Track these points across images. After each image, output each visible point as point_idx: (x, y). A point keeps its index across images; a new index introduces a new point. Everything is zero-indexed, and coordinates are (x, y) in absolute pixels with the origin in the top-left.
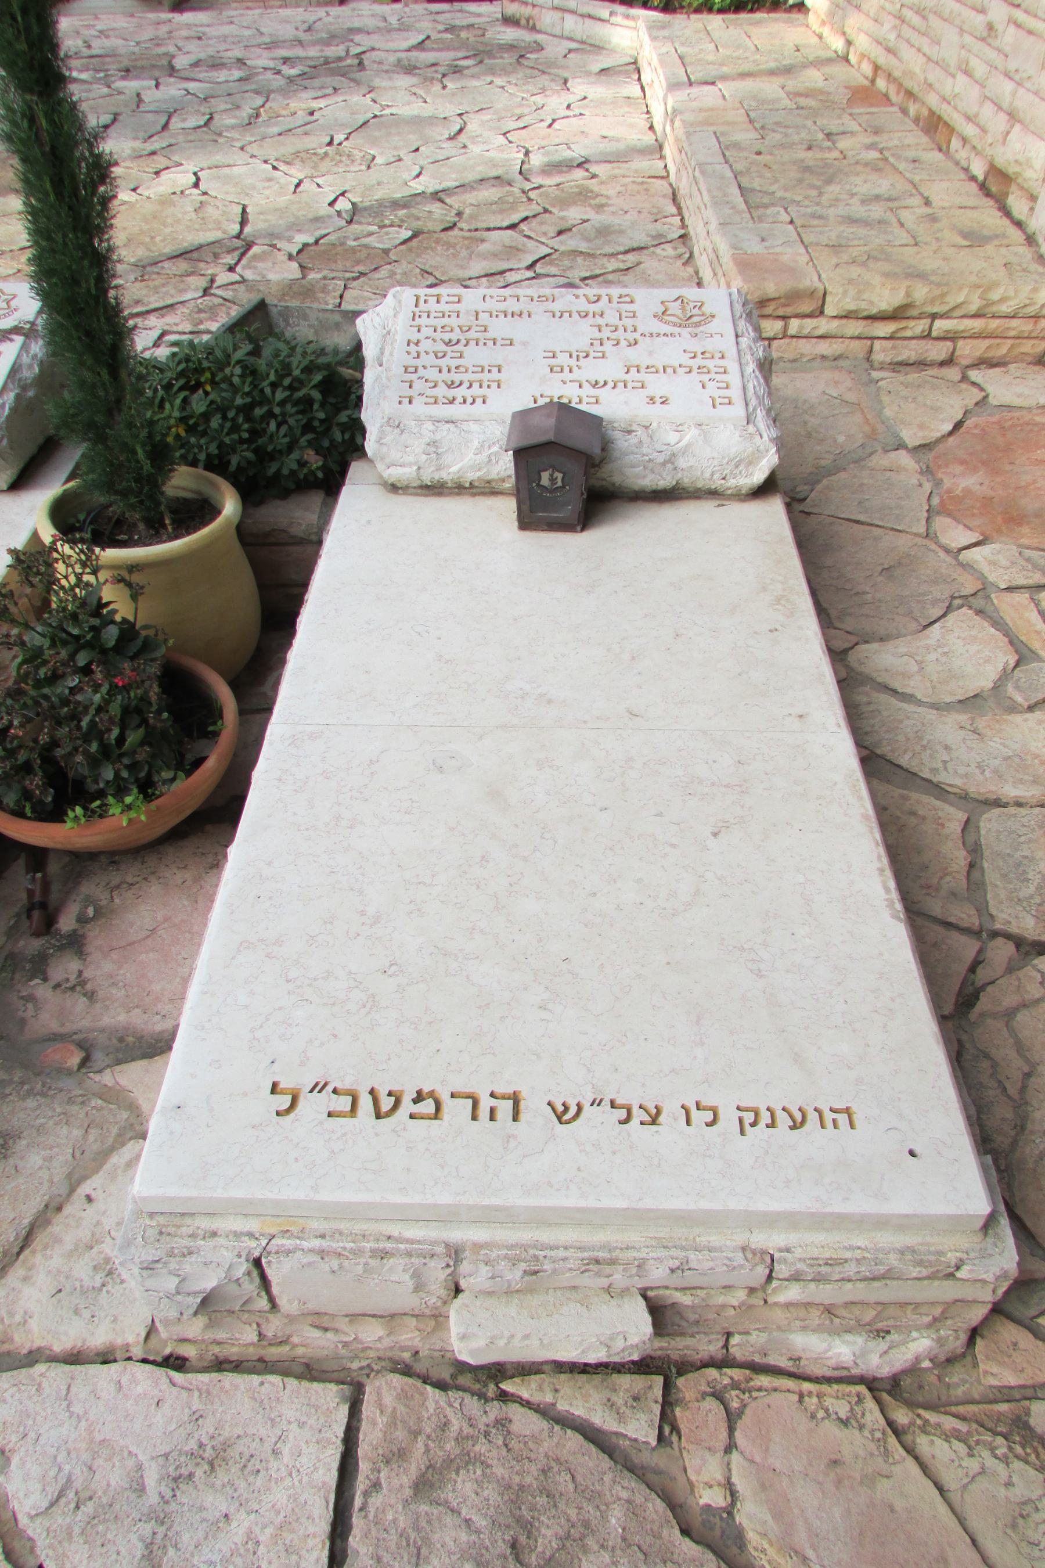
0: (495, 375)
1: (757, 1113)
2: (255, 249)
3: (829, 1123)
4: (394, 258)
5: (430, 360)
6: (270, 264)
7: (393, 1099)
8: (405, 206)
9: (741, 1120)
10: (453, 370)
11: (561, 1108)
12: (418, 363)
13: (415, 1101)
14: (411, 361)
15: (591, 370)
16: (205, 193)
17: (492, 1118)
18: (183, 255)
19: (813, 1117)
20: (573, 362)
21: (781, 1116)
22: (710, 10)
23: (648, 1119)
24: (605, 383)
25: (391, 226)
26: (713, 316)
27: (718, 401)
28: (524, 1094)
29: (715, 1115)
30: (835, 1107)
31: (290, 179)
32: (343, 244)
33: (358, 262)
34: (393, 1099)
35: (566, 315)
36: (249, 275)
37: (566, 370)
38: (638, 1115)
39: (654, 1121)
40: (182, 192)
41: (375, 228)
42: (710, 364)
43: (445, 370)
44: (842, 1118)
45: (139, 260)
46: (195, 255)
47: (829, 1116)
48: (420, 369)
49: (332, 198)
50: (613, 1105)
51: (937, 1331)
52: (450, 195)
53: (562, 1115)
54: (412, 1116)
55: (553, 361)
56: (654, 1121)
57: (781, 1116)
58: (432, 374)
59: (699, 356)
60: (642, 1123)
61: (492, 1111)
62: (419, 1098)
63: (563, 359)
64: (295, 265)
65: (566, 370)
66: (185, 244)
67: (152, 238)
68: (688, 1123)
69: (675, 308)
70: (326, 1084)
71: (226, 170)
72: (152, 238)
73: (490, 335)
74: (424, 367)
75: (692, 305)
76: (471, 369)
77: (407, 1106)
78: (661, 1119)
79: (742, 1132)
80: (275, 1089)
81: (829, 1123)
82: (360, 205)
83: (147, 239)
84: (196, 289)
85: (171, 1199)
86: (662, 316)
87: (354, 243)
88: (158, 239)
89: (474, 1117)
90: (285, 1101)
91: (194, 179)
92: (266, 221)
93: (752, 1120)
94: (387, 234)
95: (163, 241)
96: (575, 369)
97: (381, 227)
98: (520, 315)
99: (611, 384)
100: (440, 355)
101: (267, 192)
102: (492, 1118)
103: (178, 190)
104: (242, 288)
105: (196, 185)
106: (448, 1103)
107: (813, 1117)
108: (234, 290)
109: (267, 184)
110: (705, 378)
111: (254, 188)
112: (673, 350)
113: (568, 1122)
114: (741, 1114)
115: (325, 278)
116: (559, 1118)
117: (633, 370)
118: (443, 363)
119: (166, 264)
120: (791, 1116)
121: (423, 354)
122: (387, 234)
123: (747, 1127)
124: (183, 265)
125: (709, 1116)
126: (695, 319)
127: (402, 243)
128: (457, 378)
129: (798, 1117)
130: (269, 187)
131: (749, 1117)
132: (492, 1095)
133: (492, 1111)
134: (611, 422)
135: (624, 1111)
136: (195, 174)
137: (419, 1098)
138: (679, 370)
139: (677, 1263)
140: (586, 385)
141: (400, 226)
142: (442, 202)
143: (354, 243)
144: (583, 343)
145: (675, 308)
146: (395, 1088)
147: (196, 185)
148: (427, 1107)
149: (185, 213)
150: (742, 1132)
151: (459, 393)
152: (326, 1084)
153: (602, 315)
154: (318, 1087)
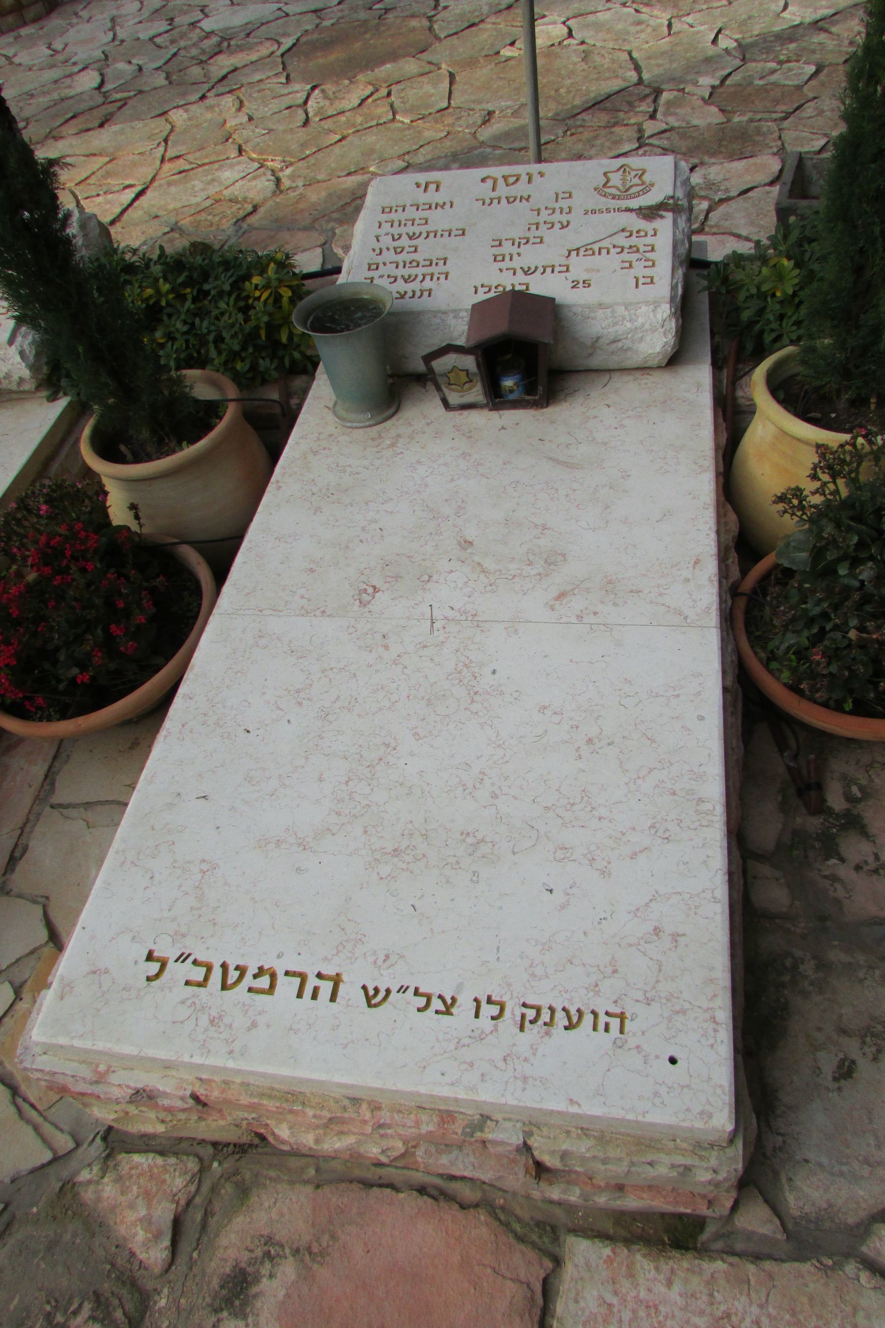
0: (441, 268)
1: (538, 1010)
2: (665, 96)
3: (601, 1026)
4: (811, 95)
5: (389, 256)
6: (689, 110)
7: (238, 973)
8: (791, 40)
9: (523, 1016)
10: (408, 265)
11: (371, 992)
12: (380, 260)
13: (255, 976)
15: (530, 256)
16: (583, 43)
17: (314, 996)
18: (597, 105)
19: (588, 1019)
20: (514, 250)
21: (560, 1015)
23: (443, 1008)
25: (788, 61)
26: (652, 185)
28: (345, 977)
29: (502, 1010)
30: (610, 1011)
31: (659, 21)
32: (751, 83)
33: (777, 102)
34: (238, 973)
36: (673, 121)
37: (507, 258)
38: (437, 1004)
39: (448, 1012)
40: (560, 43)
41: (773, 65)
42: (640, 242)
43: (401, 265)
44: (615, 1023)
45: (557, 114)
46: (608, 104)
47: (603, 1019)
48: (381, 266)
49: (712, 36)
50: (417, 992)
52: (834, 24)
53: (373, 998)
54: (250, 990)
55: (497, 251)
56: (448, 1012)
57: (560, 1015)
58: (391, 269)
60: (437, 1012)
61: (316, 990)
62: (261, 972)
63: (507, 248)
64: (714, 109)
65: (507, 258)
66: (593, 95)
67: (557, 91)
68: (477, 1015)
70: (189, 955)
71: (591, 18)
72: (557, 91)
73: (430, 227)
74: (385, 264)
75: (633, 173)
77: (248, 981)
78: (453, 1010)
79: (522, 1028)
80: (150, 957)
81: (601, 1026)
82: (744, 42)
83: (553, 93)
84: (630, 140)
86: (601, 191)
87: (761, 83)
88: (562, 91)
89: (300, 995)
90: (155, 967)
91: (566, 30)
92: (659, 66)
93: (532, 1018)
94: (790, 70)
95: (568, 92)
96: (515, 257)
97: (781, 63)
98: (442, 207)
99: (541, 270)
100: (399, 250)
101: (643, 36)
102: (314, 996)
103: (556, 41)
104: (674, 136)
105: (570, 35)
106: (281, 979)
107: (588, 1019)
108: (668, 139)
109: (639, 28)
110: (633, 257)
111: (628, 33)
113: (376, 1005)
114: (524, 1010)
115: (751, 121)
116: (368, 999)
118: (400, 258)
119: (584, 116)
120: (569, 1018)
121: (384, 250)
122: (790, 70)
123: (527, 1023)
124: (602, 118)
125: (495, 1010)
127: (810, 79)
129: (575, 1019)
130: (642, 31)
131: (531, 1014)
132: (607, 1013)
133: (316, 990)
134: (568, 306)
135: (424, 999)
136: (605, 174)
137: (261, 972)
140: (519, 272)
141: (798, 61)
142: (826, 31)
143: (761, 83)
144: (517, 233)
145: (616, 179)
146: (241, 963)
147: (570, 35)
148: (264, 982)
149: (575, 64)
150: (522, 1028)
152: (189, 955)
153: (527, 200)
154: (182, 958)
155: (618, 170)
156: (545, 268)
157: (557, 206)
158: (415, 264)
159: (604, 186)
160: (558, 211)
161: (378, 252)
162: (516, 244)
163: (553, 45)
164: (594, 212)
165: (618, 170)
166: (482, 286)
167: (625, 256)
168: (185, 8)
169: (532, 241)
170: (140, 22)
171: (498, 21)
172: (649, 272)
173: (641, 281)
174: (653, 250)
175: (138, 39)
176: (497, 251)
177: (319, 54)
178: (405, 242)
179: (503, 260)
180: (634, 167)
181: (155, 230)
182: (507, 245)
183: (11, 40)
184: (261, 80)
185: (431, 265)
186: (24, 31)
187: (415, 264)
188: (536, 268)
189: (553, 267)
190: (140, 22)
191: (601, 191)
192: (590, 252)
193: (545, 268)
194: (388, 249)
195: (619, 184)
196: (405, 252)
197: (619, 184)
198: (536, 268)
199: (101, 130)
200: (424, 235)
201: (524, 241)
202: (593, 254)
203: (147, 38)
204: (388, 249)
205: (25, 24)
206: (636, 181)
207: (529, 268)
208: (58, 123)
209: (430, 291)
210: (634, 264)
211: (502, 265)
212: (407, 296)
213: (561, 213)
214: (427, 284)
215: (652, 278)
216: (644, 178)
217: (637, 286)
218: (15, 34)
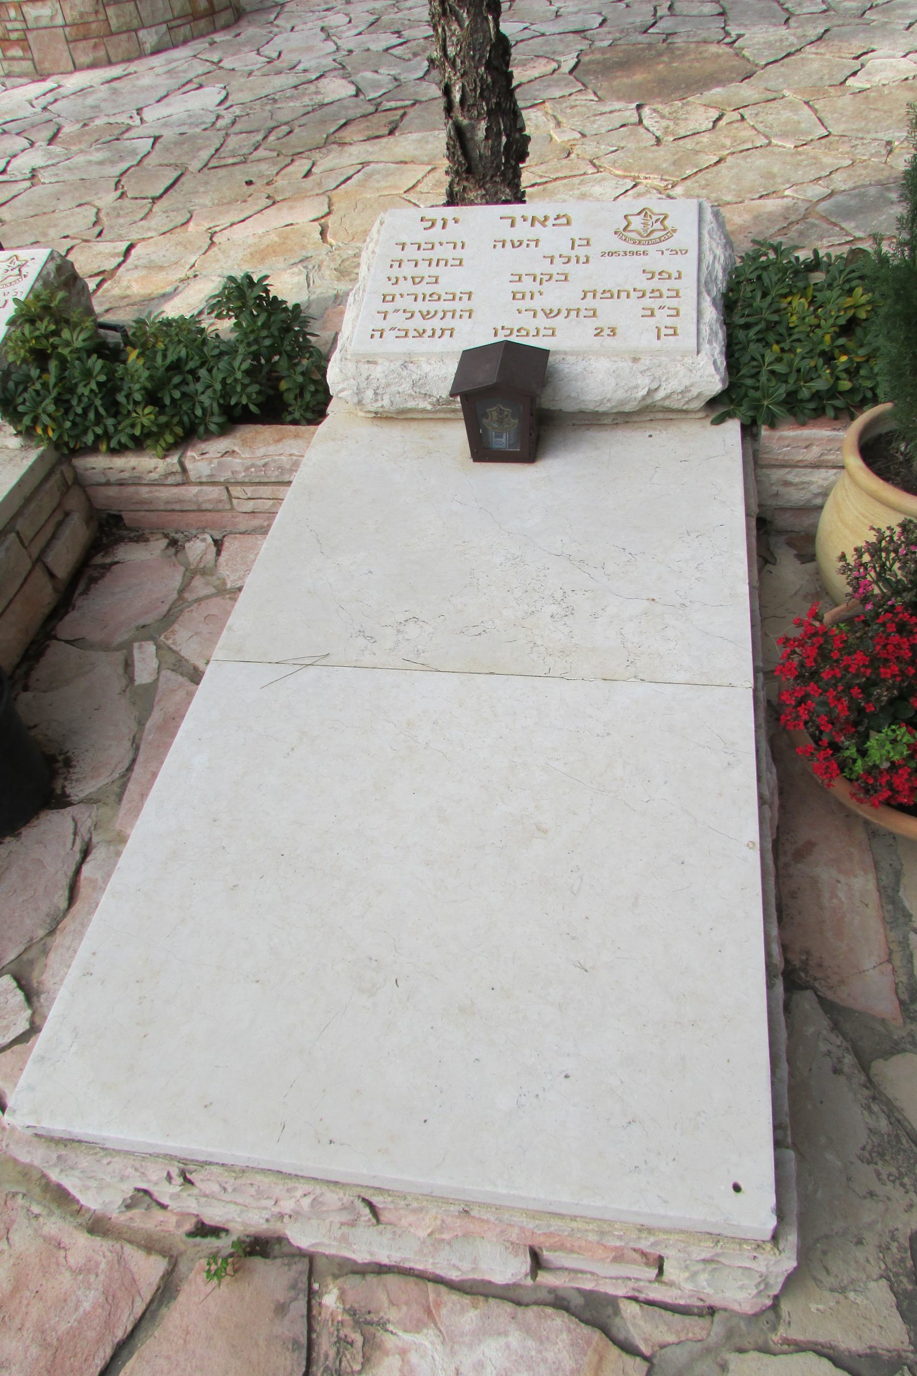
0: (465, 304)
5: (406, 287)
10: (428, 298)
12: (396, 290)
14: (390, 289)
20: (535, 287)
22: (146, 56)
24: (559, 312)
26: (674, 231)
27: (664, 331)
35: (442, 263)
42: (664, 286)
43: (420, 297)
48: (398, 297)
51: (609, 1317)
59: (657, 277)
63: (527, 285)
65: (528, 296)
69: (637, 223)
75: (655, 218)
76: (444, 296)
85: (150, 1145)
86: (622, 233)
96: (537, 295)
99: (565, 313)
100: (417, 280)
110: (655, 304)
112: (626, 272)
117: (590, 295)
126: (656, 235)
128: (432, 306)
138: (632, 293)
139: (865, 1112)
140: (540, 314)
145: (637, 223)
151: (428, 325)
155: (639, 214)
156: (569, 311)
157: (573, 254)
158: (435, 297)
159: (624, 230)
160: (574, 260)
161: (394, 280)
162: (538, 280)
163: (906, 79)
164: (611, 254)
165: (639, 214)
166: (503, 328)
167: (647, 302)
168: (406, 22)
169: (555, 277)
170: (360, 34)
171: (822, 51)
172: (670, 322)
173: (577, 242)
174: (677, 296)
175: (368, 50)
176: (517, 287)
177: (618, 74)
178: (423, 270)
179: (523, 298)
180: (656, 211)
181: (722, 283)
182: (528, 280)
183: (207, 45)
184: (563, 97)
185: (454, 299)
186: (218, 37)
187: (435, 297)
188: (436, 312)
189: (578, 310)
190: (360, 34)
191: (622, 233)
192: (608, 295)
193: (569, 311)
194: (405, 279)
195: (640, 228)
196: (424, 282)
197: (640, 228)
198: (436, 312)
199: (392, 139)
200: (441, 314)
201: (547, 277)
202: (612, 297)
203: (381, 49)
204: (405, 279)
205: (215, 31)
206: (658, 226)
207: (428, 313)
208: (332, 130)
209: (452, 330)
210: (656, 312)
211: (520, 304)
212: (425, 335)
213: (578, 262)
214: (448, 323)
215: (675, 329)
216: (666, 223)
217: (659, 338)
218: (208, 39)
